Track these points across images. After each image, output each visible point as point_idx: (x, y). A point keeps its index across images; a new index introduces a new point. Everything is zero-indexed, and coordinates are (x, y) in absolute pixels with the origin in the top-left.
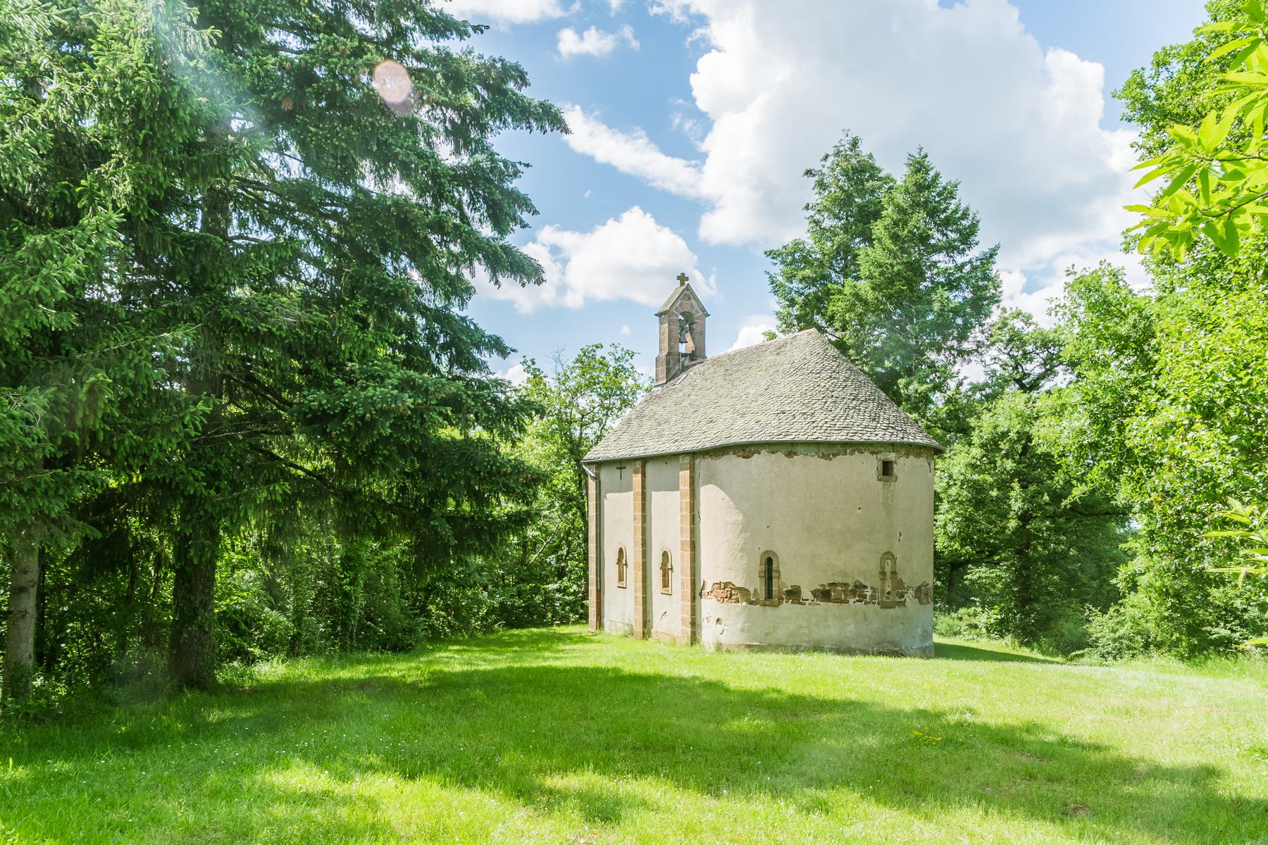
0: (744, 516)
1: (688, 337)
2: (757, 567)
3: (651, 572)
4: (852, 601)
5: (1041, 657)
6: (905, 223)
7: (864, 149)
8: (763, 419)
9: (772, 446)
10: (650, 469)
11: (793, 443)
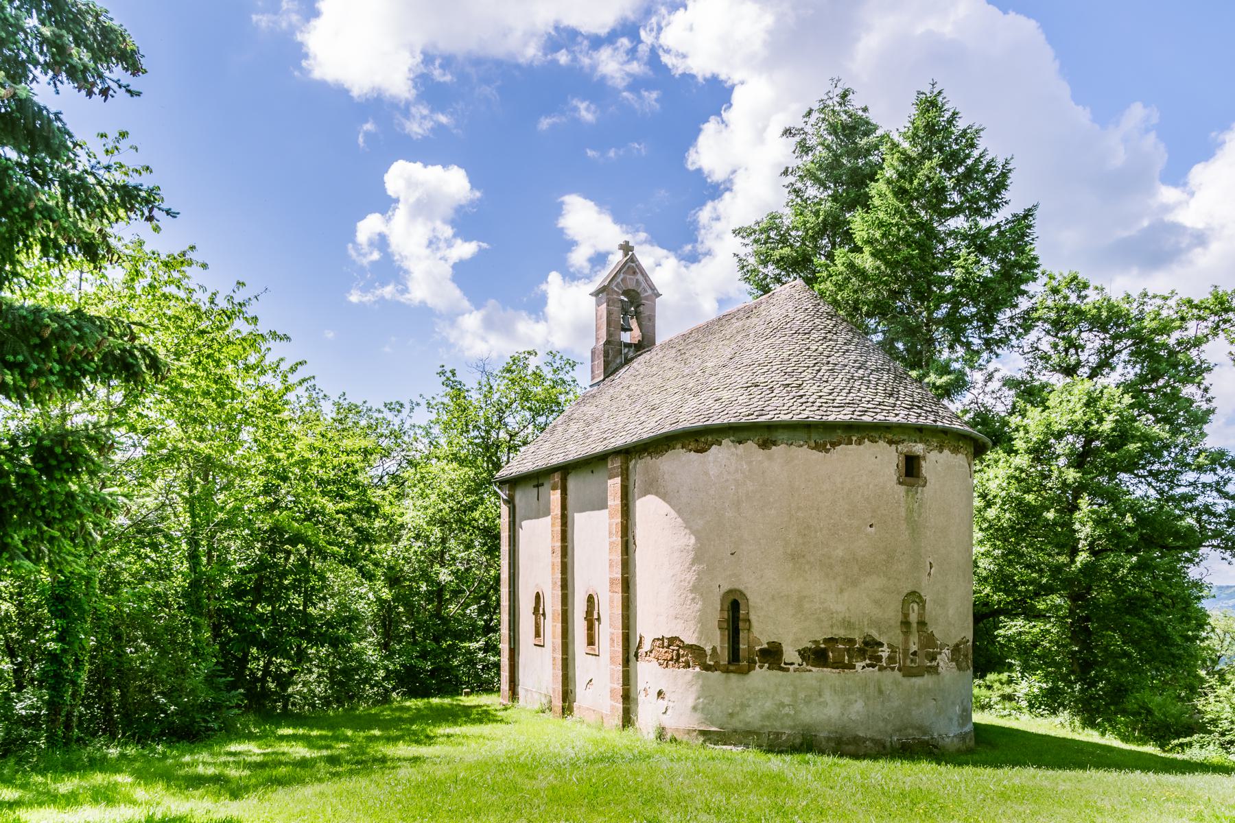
0: (697, 539)
1: (634, 324)
2: (716, 614)
3: (572, 620)
4: (859, 665)
5: (1060, 726)
6: (914, 175)
7: (856, 103)
8: (725, 395)
9: (737, 432)
10: (572, 484)
11: (771, 427)
